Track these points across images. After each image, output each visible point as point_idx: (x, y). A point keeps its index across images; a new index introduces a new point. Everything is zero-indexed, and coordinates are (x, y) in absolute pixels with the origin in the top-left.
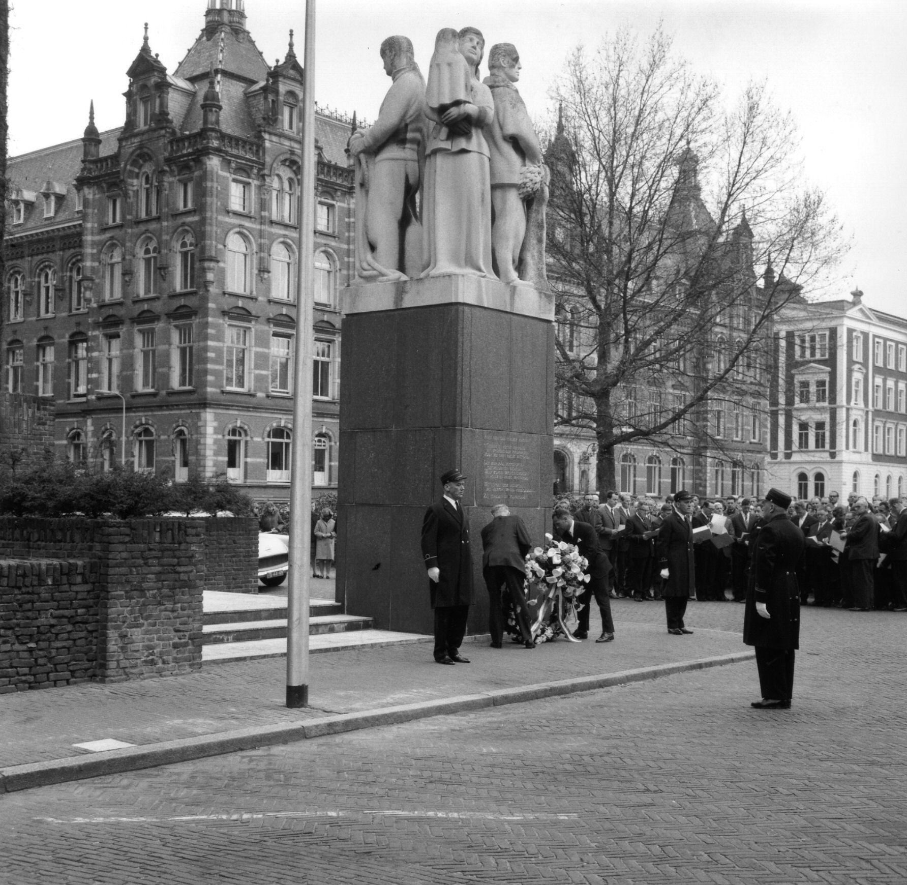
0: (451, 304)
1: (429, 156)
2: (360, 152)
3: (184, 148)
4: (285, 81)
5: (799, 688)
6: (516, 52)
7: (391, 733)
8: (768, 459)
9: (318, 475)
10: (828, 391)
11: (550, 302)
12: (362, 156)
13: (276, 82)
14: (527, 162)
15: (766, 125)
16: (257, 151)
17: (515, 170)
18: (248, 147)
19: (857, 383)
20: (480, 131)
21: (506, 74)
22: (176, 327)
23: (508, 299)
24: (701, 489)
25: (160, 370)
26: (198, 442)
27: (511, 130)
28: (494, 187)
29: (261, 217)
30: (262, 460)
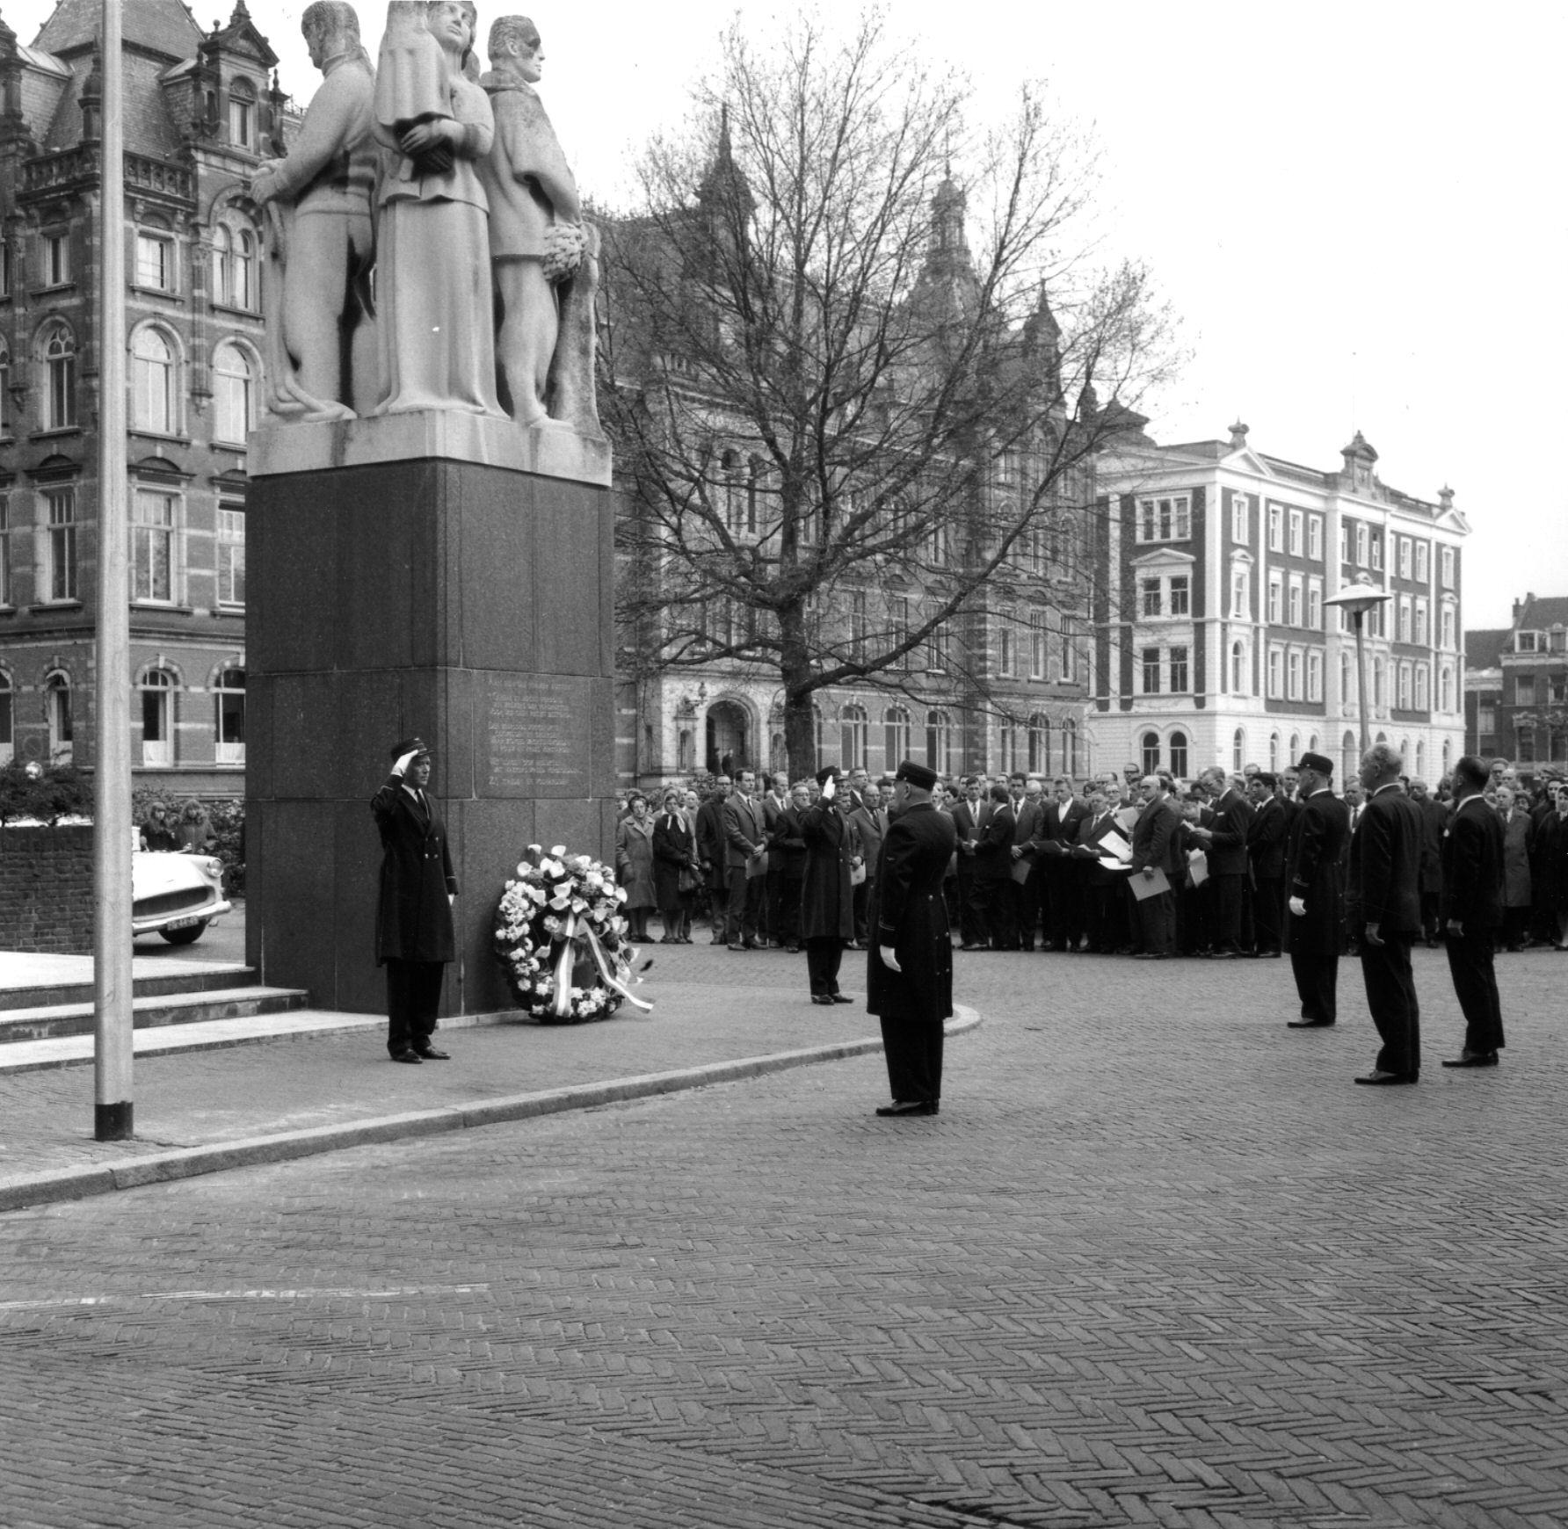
0: (424, 460)
1: (385, 207)
2: (269, 199)
3: (50, 177)
4: (231, 59)
5: (951, 1086)
6: (534, 31)
7: (263, 1177)
8: (1090, 708)
9: (150, 747)
10: (1189, 595)
11: (603, 455)
12: (272, 206)
13: (214, 61)
14: (557, 220)
15: (1055, 145)
16: (184, 182)
17: (531, 230)
18: (166, 176)
19: (1240, 583)
20: (469, 167)
21: (519, 68)
22: (45, 493)
23: (526, 449)
24: (977, 762)
25: (19, 570)
26: (87, 696)
27: (525, 164)
28: (498, 263)
29: (194, 299)
30: (207, 727)
